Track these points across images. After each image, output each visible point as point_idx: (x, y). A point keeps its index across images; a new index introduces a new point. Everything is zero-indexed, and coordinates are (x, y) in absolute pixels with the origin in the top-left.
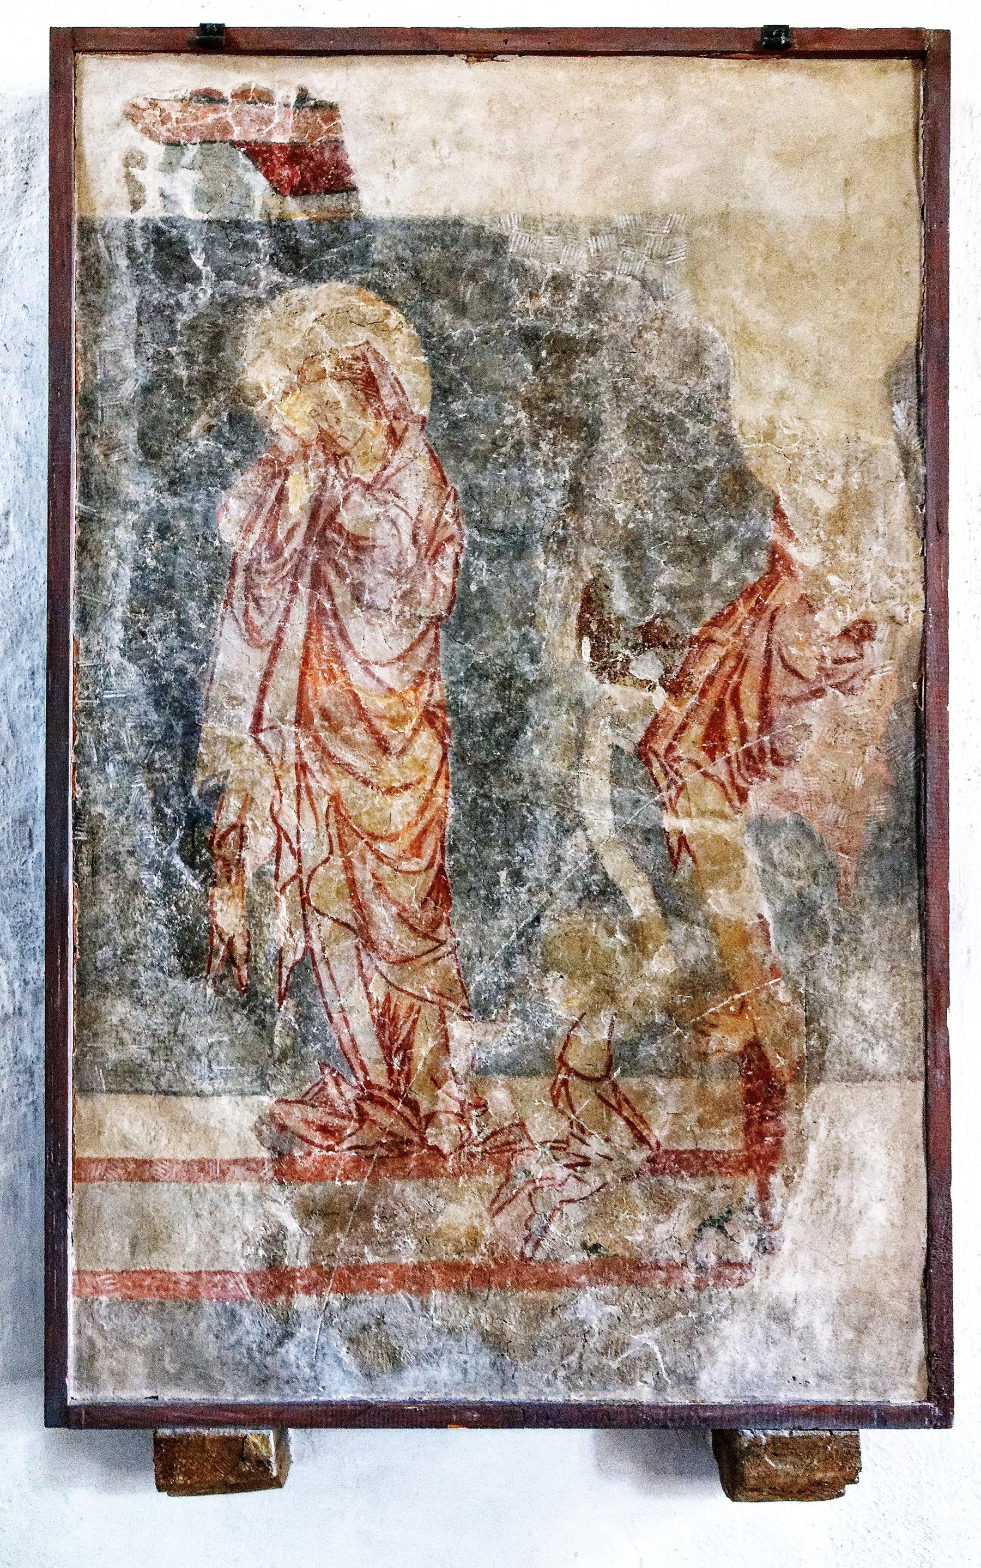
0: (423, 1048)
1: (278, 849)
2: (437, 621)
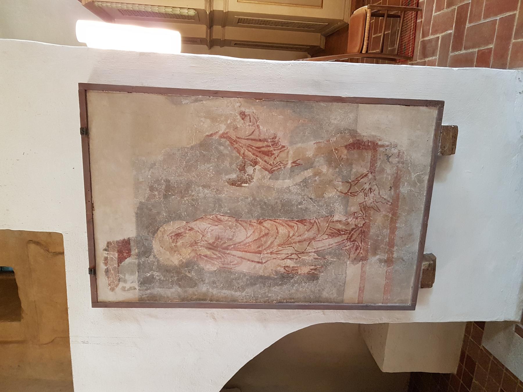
0: (340, 226)
1: (290, 259)
2: (237, 221)
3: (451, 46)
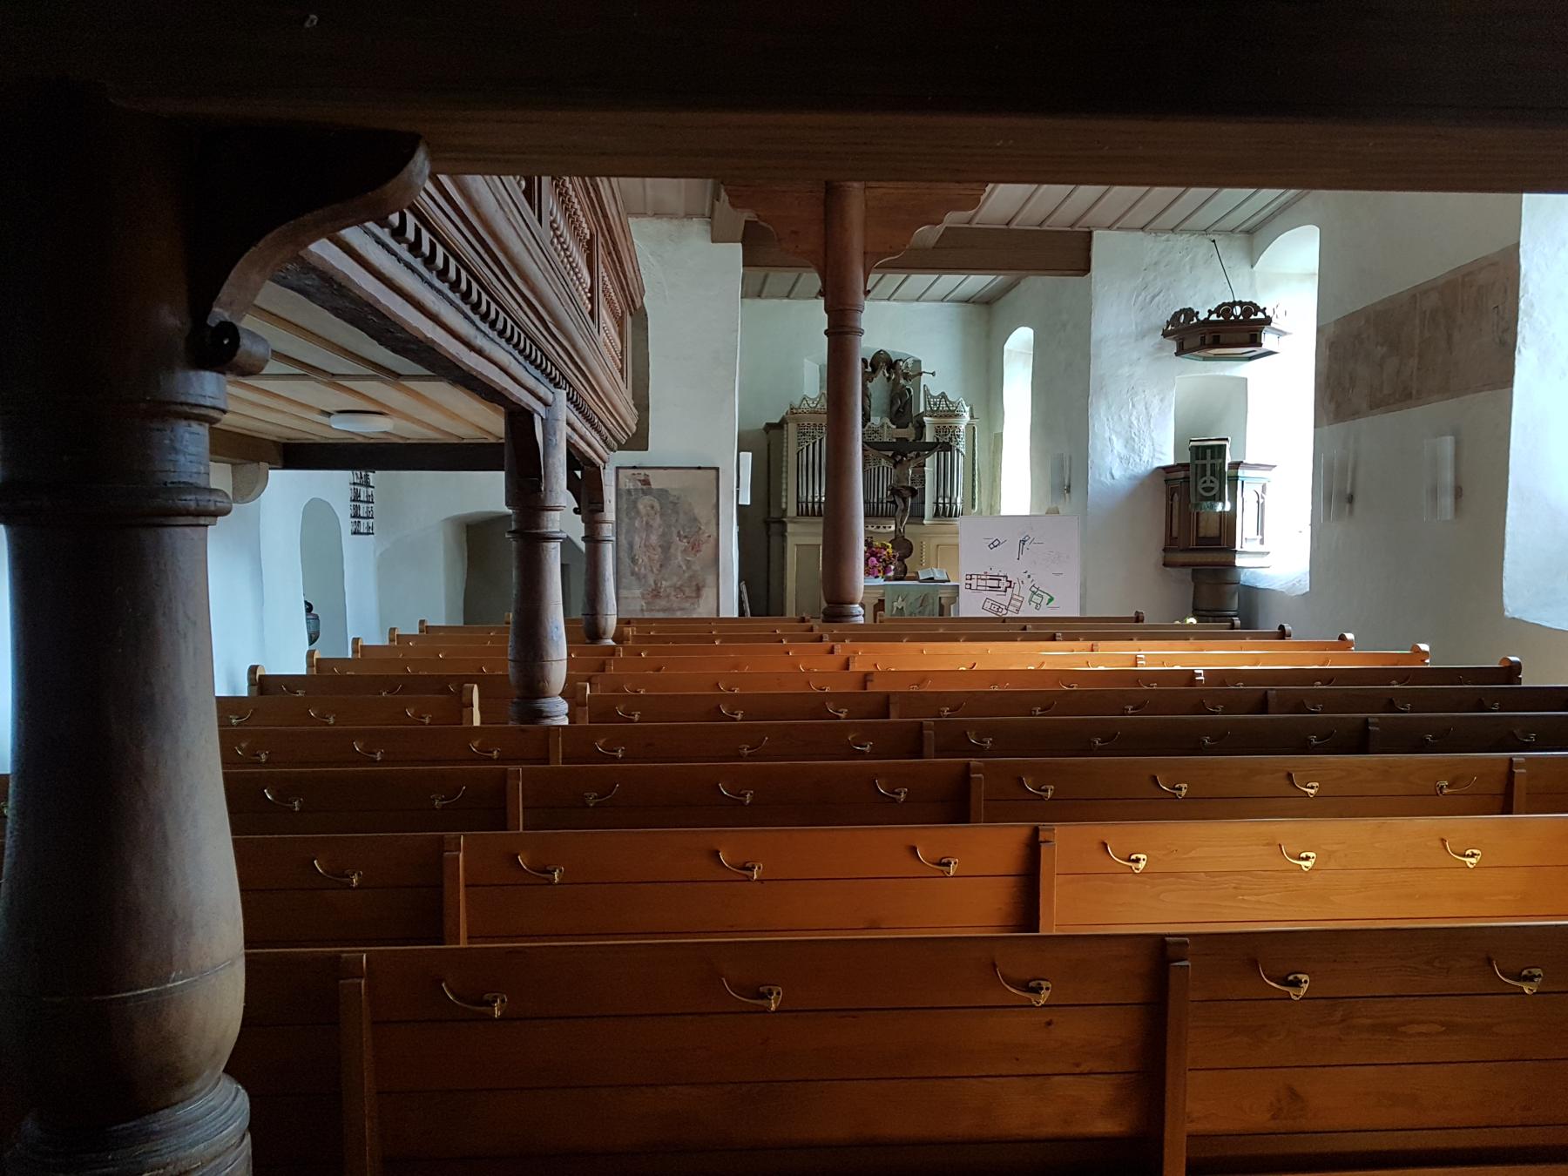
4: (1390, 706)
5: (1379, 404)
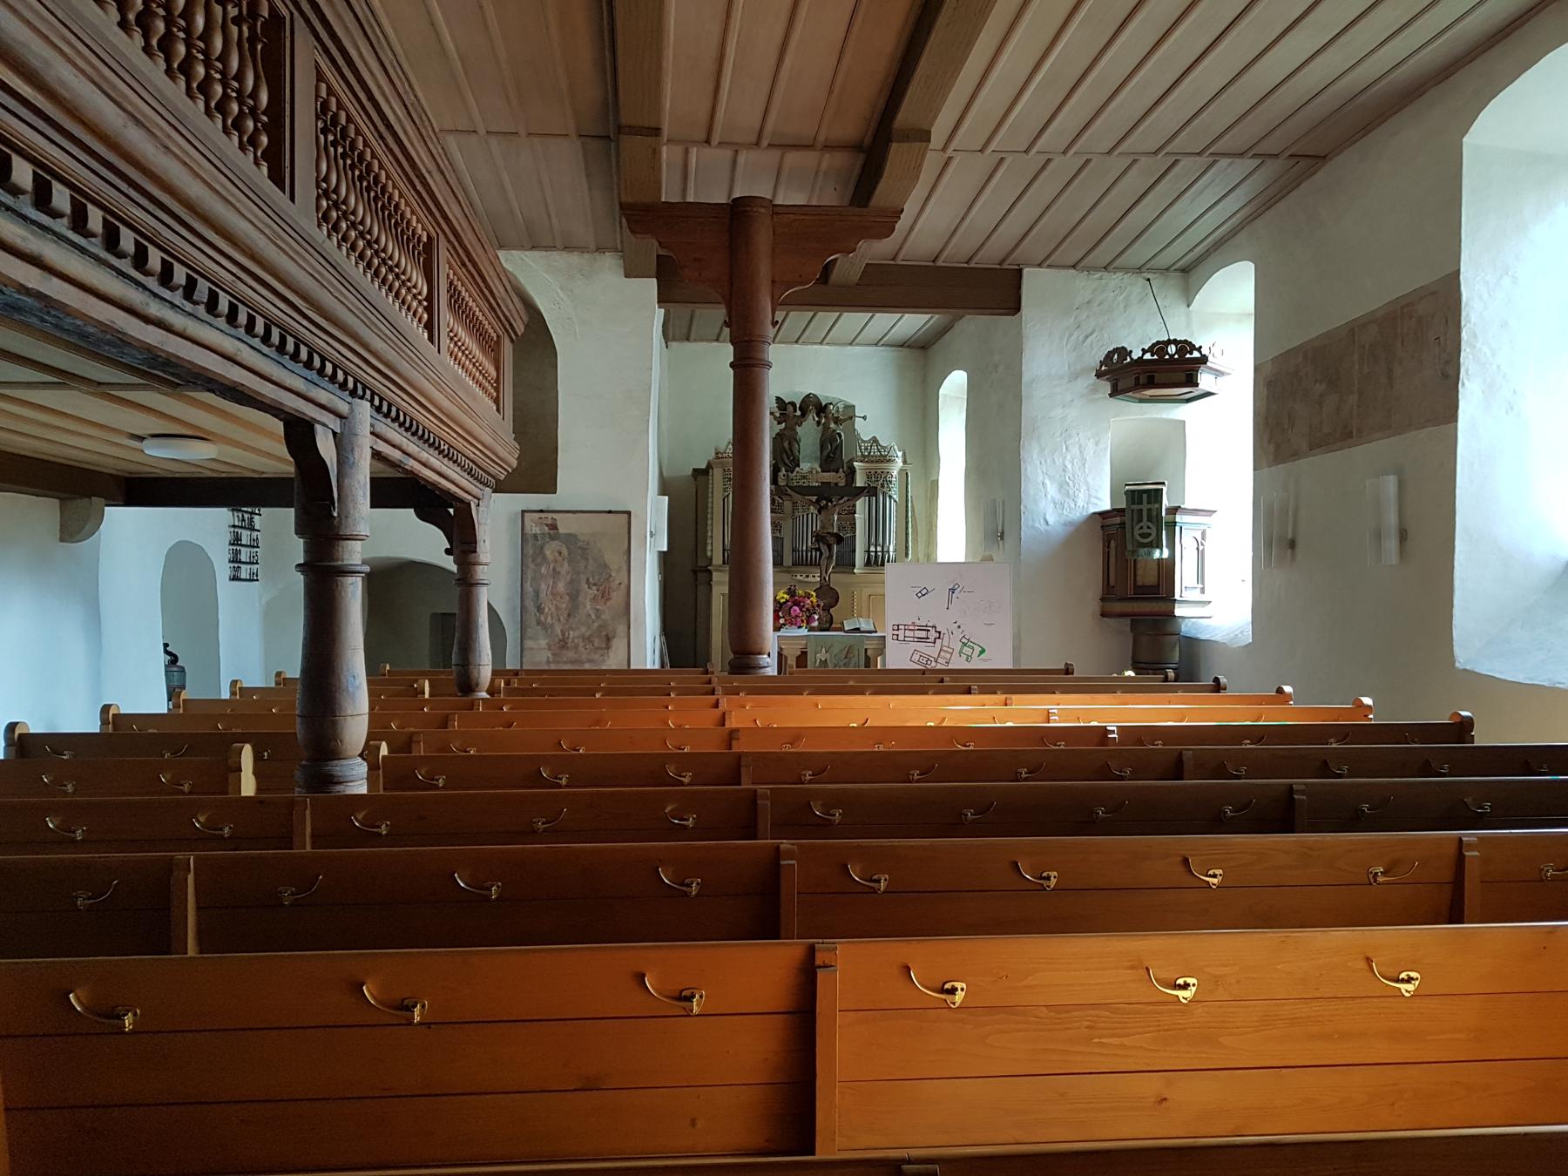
3: (255, 234)
4: (1324, 770)
5: (1321, 442)
